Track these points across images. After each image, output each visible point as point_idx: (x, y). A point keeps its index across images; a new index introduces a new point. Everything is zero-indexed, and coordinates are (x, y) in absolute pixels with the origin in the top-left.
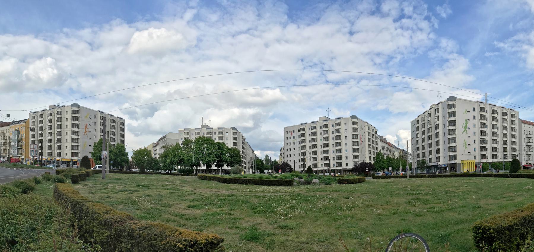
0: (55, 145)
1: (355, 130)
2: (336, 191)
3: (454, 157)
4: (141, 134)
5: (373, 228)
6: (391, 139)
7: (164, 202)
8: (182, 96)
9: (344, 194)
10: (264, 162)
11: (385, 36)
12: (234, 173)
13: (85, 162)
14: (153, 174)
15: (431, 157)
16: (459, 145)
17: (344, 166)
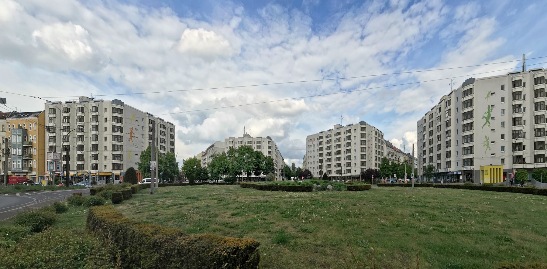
0: (88, 154)
1: (363, 135)
2: (346, 198)
3: (471, 162)
4: (191, 143)
5: (376, 238)
6: (397, 143)
7: (211, 212)
8: (228, 104)
9: (352, 201)
10: (291, 169)
11: (392, 31)
12: (268, 180)
13: (131, 175)
14: (202, 184)
15: (439, 161)
16: (478, 144)
17: (353, 173)
